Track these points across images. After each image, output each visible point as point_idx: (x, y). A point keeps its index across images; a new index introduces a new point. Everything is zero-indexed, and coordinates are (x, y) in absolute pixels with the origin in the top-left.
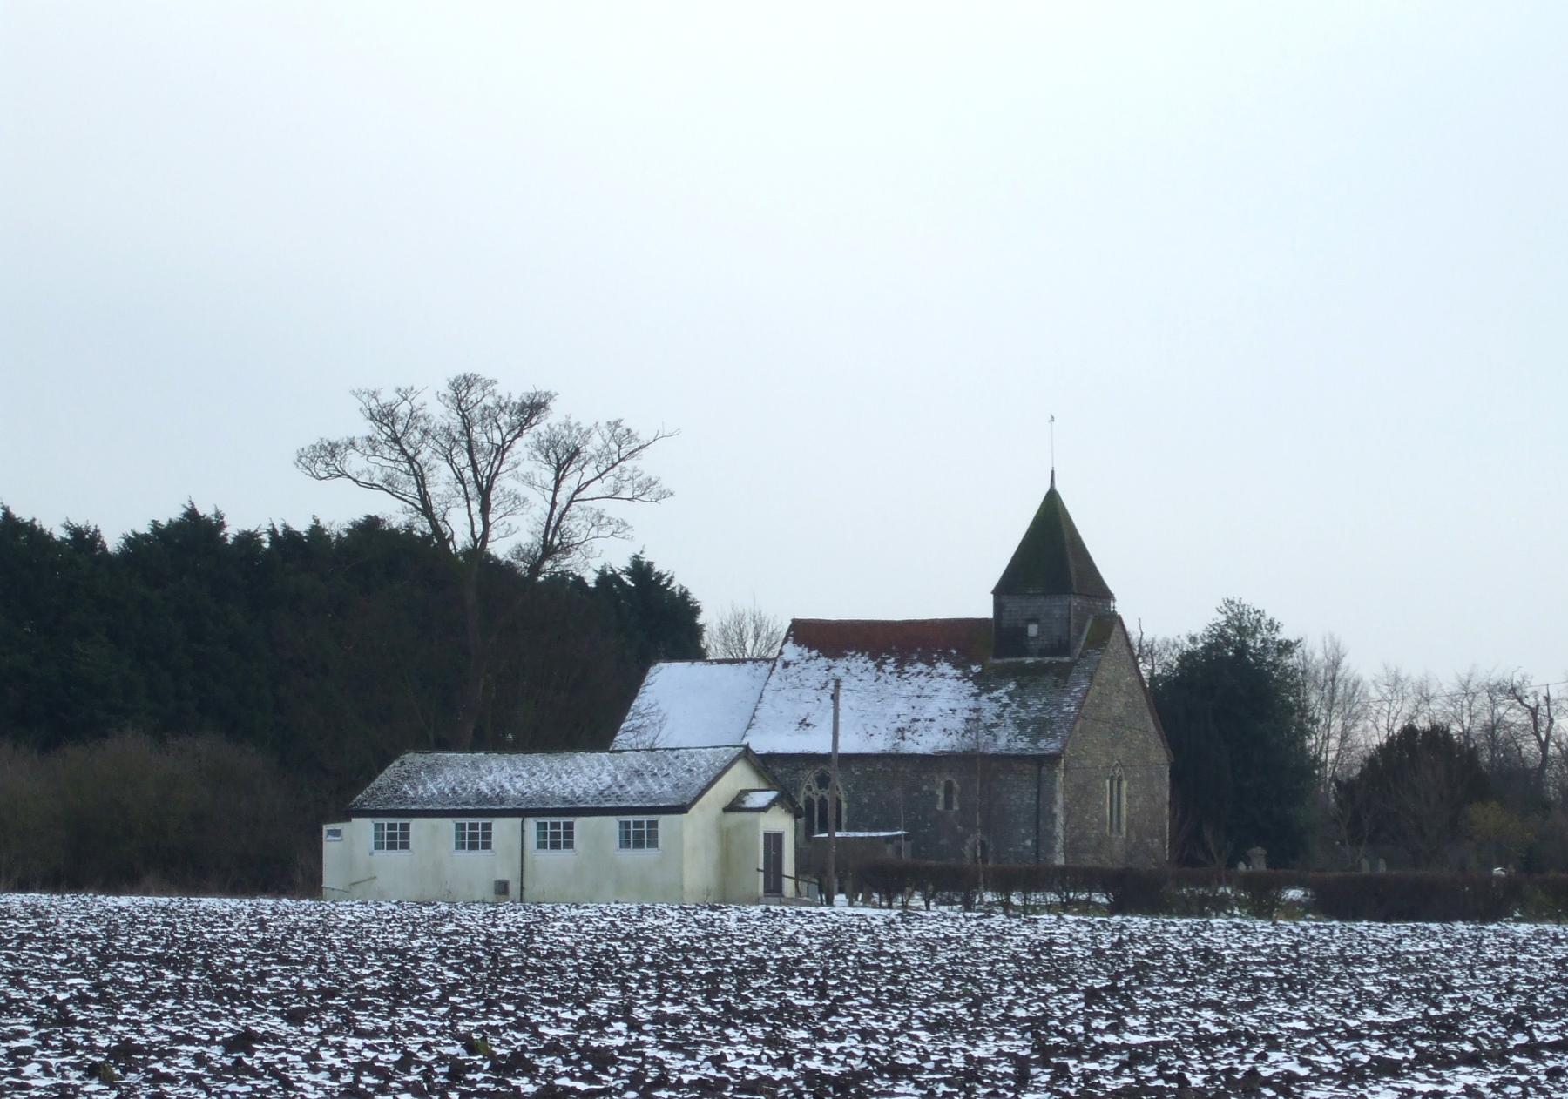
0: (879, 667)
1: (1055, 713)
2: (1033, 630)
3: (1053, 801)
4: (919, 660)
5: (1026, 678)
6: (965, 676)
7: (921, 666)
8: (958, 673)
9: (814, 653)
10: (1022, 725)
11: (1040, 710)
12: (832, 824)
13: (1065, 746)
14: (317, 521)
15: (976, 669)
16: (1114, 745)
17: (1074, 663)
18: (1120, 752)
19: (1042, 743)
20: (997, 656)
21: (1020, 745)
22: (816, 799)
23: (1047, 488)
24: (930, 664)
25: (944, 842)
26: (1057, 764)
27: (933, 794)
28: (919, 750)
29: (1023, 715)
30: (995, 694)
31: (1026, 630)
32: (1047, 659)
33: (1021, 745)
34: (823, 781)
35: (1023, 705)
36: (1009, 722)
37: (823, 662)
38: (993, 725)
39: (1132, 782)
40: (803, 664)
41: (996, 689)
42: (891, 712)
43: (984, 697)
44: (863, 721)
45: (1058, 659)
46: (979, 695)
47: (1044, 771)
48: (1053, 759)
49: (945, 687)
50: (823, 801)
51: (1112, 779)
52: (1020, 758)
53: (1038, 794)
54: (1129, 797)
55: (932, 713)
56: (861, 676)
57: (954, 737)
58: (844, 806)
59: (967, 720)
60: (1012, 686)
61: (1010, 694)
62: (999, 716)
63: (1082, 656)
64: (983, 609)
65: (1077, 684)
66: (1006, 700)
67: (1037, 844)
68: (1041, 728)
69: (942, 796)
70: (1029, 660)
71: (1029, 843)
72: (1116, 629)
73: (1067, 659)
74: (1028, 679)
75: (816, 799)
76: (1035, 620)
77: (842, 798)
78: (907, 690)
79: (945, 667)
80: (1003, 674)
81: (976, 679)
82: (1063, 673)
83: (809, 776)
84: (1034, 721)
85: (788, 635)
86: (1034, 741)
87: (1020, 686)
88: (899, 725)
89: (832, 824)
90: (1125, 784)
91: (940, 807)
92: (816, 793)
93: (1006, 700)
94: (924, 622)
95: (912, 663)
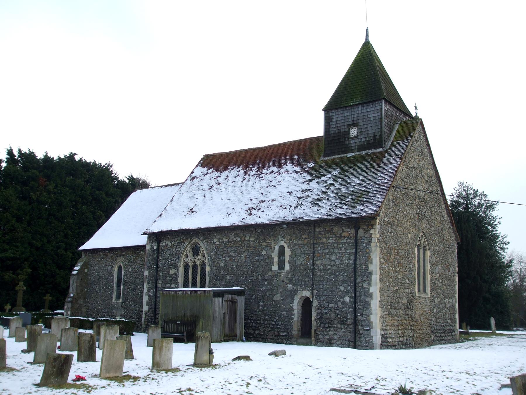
0: (246, 173)
1: (370, 186)
2: (353, 132)
3: (369, 260)
4: (273, 165)
5: (348, 166)
6: (303, 171)
7: (273, 169)
8: (298, 169)
9: (211, 170)
10: (342, 197)
11: (358, 185)
12: (198, 284)
13: (380, 208)
14: (47, 154)
15: (310, 165)
16: (420, 220)
17: (387, 151)
18: (424, 226)
19: (359, 208)
20: (324, 156)
21: (339, 211)
22: (190, 264)
23: (363, 41)
24: (280, 166)
25: (278, 297)
26: (372, 226)
27: (269, 257)
28: (259, 221)
29: (344, 190)
30: (323, 179)
31: (348, 133)
32: (364, 153)
33: (342, 211)
34: (196, 251)
35: (346, 184)
36: (332, 196)
37: (215, 174)
38: (318, 200)
39: (433, 254)
40: (203, 177)
41: (324, 176)
42: (247, 198)
43: (314, 182)
44: (227, 205)
45: (373, 151)
46: (311, 180)
47: (361, 232)
48: (369, 221)
49: (287, 179)
50: (195, 266)
51: (419, 247)
52: (340, 221)
53: (356, 253)
54: (431, 264)
55: (283, 196)
56: (234, 179)
57: (287, 211)
58: (208, 269)
59: (299, 198)
60: (336, 172)
61: (335, 179)
62: (324, 193)
63: (391, 146)
64: (318, 131)
65: (388, 164)
66: (331, 181)
67: (355, 299)
68: (359, 197)
69: (276, 260)
70: (349, 155)
71: (347, 299)
72: (419, 128)
73: (380, 150)
74: (346, 166)
75: (190, 264)
76: (354, 124)
77: (207, 263)
78: (261, 183)
79: (290, 167)
80: (329, 166)
81: (310, 171)
82: (378, 159)
83: (187, 247)
84: (352, 193)
85: (199, 163)
86: (352, 207)
87: (343, 171)
88: (250, 206)
89: (198, 284)
90: (428, 253)
91: (275, 268)
92: (191, 260)
93: (331, 181)
94: (280, 145)
95: (268, 168)
